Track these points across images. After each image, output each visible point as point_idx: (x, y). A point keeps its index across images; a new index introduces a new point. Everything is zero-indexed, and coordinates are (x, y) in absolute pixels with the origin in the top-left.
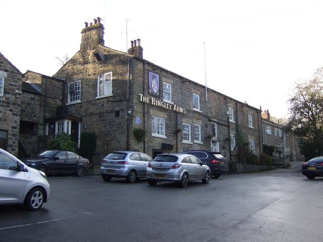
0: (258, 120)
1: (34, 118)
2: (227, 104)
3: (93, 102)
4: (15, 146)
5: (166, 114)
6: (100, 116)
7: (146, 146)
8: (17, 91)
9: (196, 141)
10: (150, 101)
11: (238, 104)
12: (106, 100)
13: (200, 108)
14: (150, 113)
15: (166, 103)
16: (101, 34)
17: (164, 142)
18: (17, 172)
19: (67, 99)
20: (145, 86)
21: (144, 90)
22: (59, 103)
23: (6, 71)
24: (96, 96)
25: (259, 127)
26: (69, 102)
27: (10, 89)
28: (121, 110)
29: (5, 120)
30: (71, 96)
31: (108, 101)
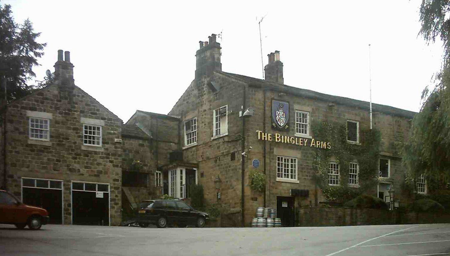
3: (210, 144)
4: (118, 199)
8: (116, 140)
10: (273, 137)
14: (273, 152)
15: (298, 138)
16: (216, 56)
17: (295, 187)
22: (174, 146)
23: (103, 119)
26: (186, 145)
27: (108, 139)
28: (236, 152)
30: (188, 138)
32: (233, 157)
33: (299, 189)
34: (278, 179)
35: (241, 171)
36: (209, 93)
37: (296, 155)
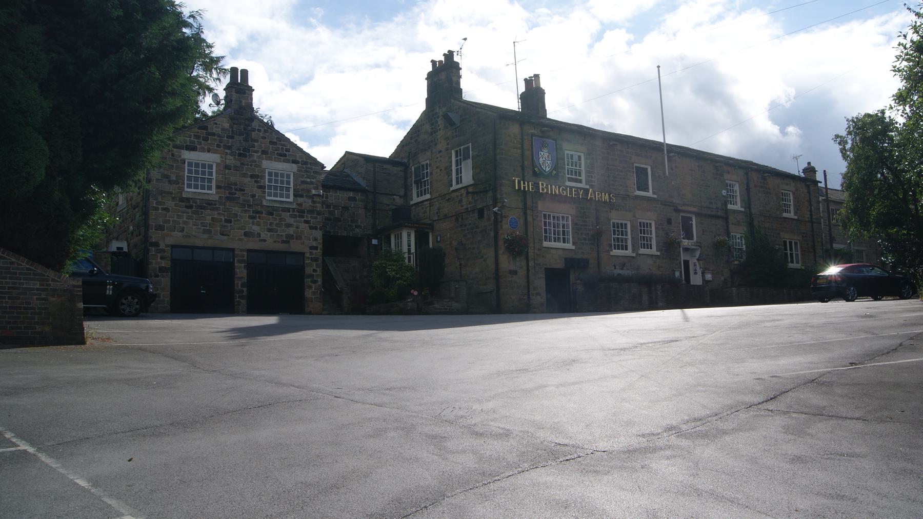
0: (810, 201)
1: (357, 230)
2: (722, 176)
7: (531, 264)
8: (314, 192)
9: (642, 251)
14: (537, 207)
15: (571, 188)
19: (412, 195)
20: (526, 163)
22: (399, 201)
23: (294, 162)
24: (451, 185)
25: (811, 215)
26: (416, 199)
28: (485, 206)
29: (299, 238)
30: (418, 188)
31: (468, 193)
32: (481, 215)
34: (546, 244)
35: (492, 234)
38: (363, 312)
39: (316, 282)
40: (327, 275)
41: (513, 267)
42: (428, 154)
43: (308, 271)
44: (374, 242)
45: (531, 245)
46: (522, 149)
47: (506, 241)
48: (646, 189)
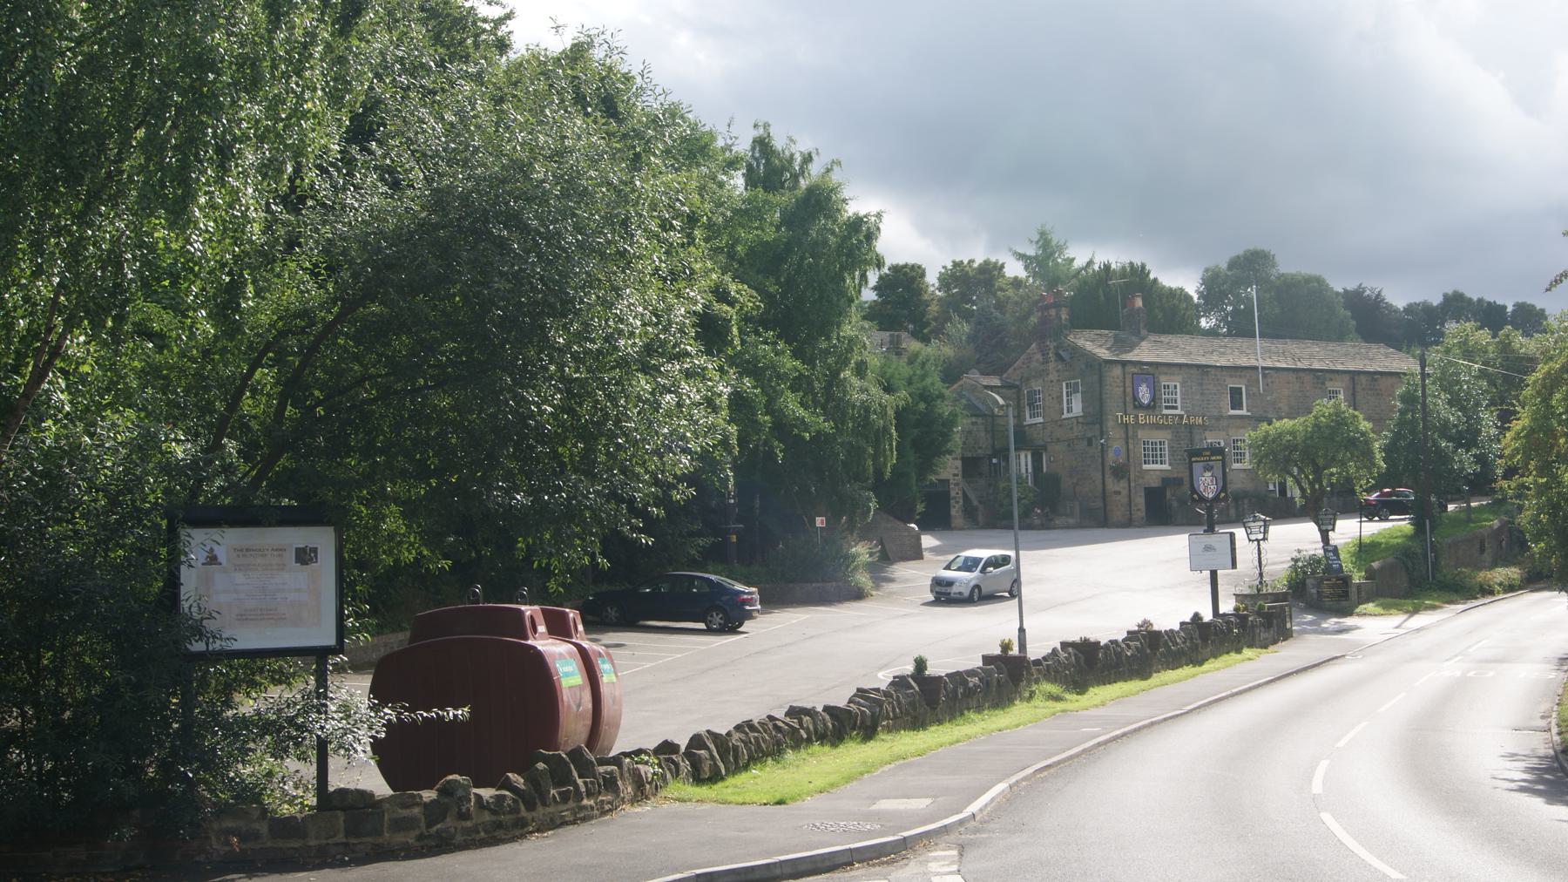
1: (980, 451)
3: (1059, 423)
5: (1169, 431)
6: (1069, 445)
7: (1132, 484)
11: (1363, 379)
12: (1074, 421)
13: (1247, 406)
15: (1167, 416)
18: (973, 529)
21: (1125, 403)
32: (1090, 443)
33: (1172, 476)
34: (1145, 467)
35: (1100, 460)
36: (1056, 361)
37: (1164, 437)
38: (994, 527)
39: (957, 502)
40: (965, 497)
41: (1117, 489)
42: (1041, 381)
43: (953, 494)
44: (994, 461)
45: (1132, 469)
46: (1125, 387)
47: (1112, 468)
48: (1240, 407)
